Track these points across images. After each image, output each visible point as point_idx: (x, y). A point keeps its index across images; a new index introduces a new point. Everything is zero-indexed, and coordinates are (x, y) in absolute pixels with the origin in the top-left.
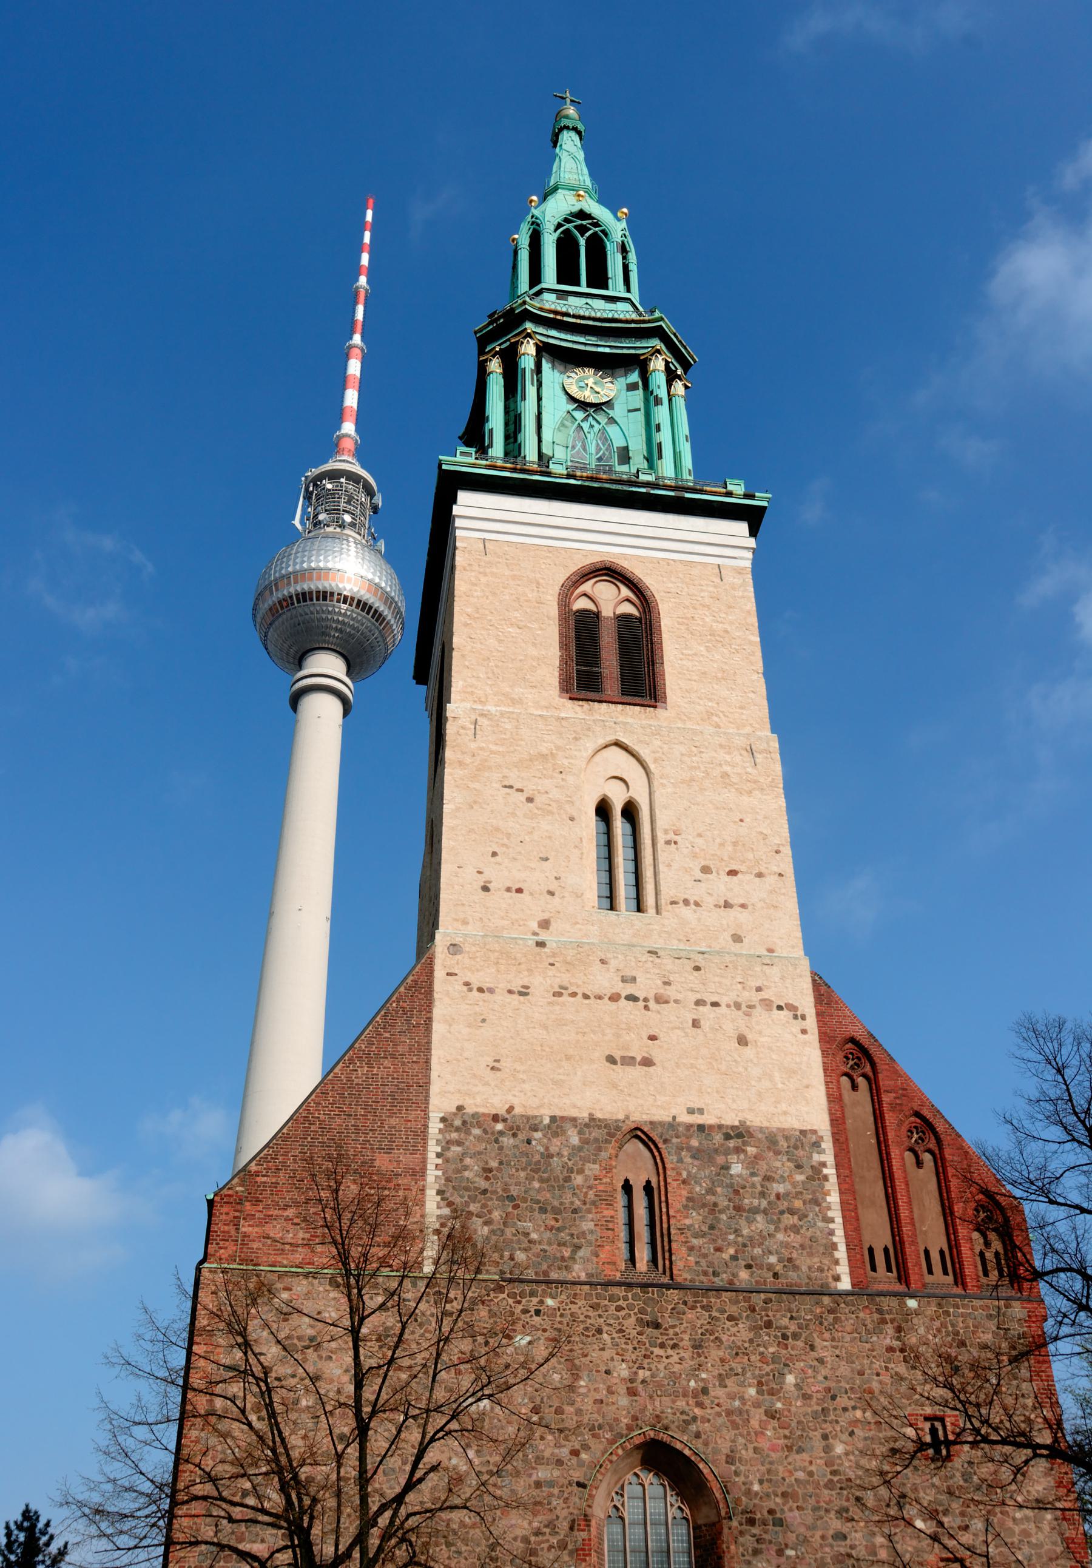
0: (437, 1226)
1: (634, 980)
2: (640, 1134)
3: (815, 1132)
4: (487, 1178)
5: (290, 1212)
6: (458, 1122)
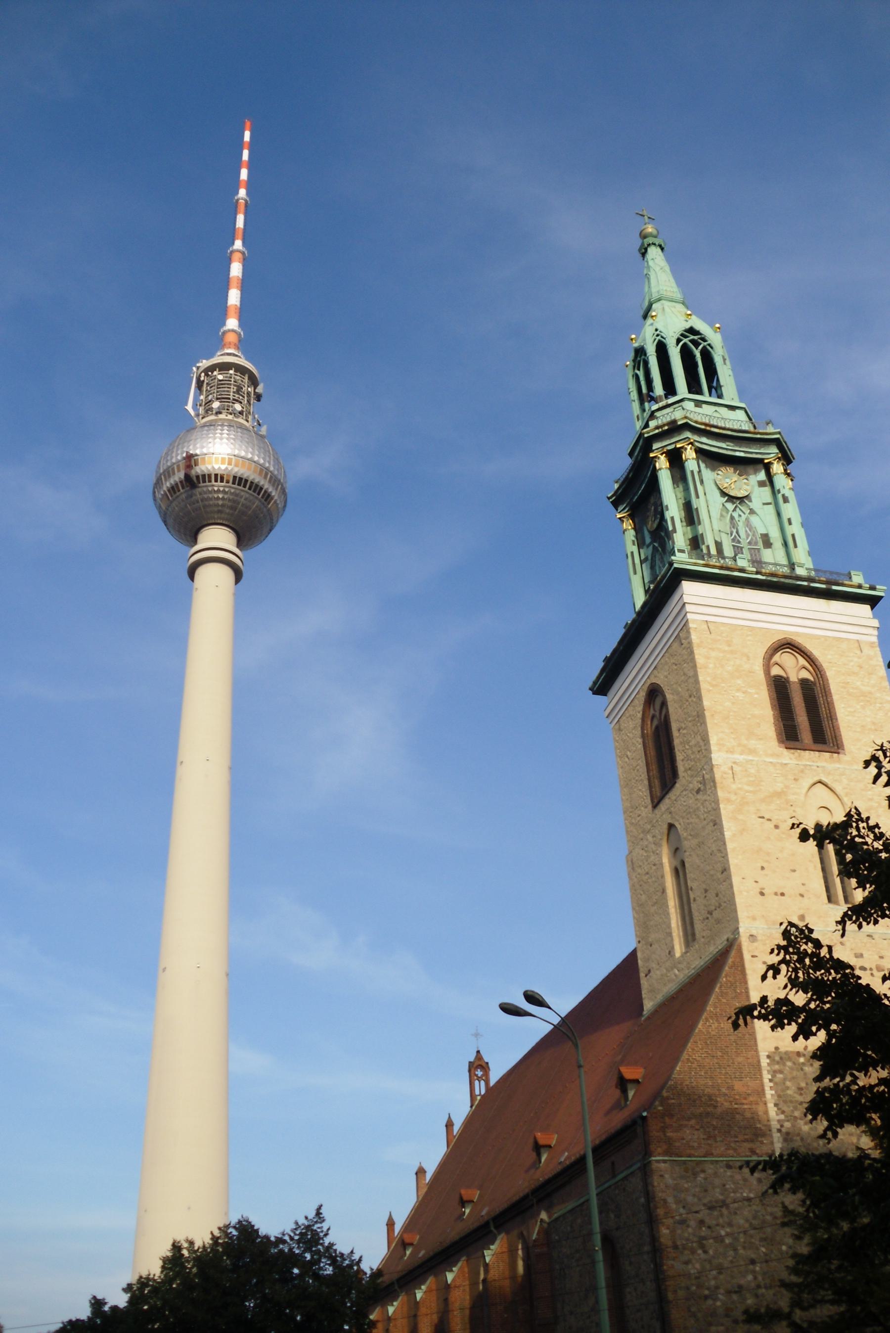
0: (779, 1127)
1: (861, 956)
4: (801, 1094)
5: (693, 1122)
6: (777, 1058)
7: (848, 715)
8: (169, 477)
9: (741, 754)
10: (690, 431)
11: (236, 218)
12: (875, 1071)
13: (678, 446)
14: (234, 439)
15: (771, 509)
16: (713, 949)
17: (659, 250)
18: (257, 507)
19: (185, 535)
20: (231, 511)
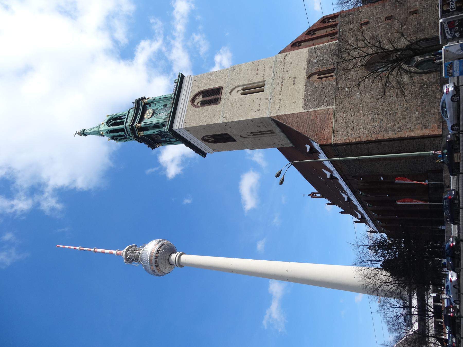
0: (325, 107)
2: (309, 77)
3: (309, 50)
4: (316, 100)
5: (322, 131)
6: (306, 107)
13: (137, 128)
16: (275, 125)
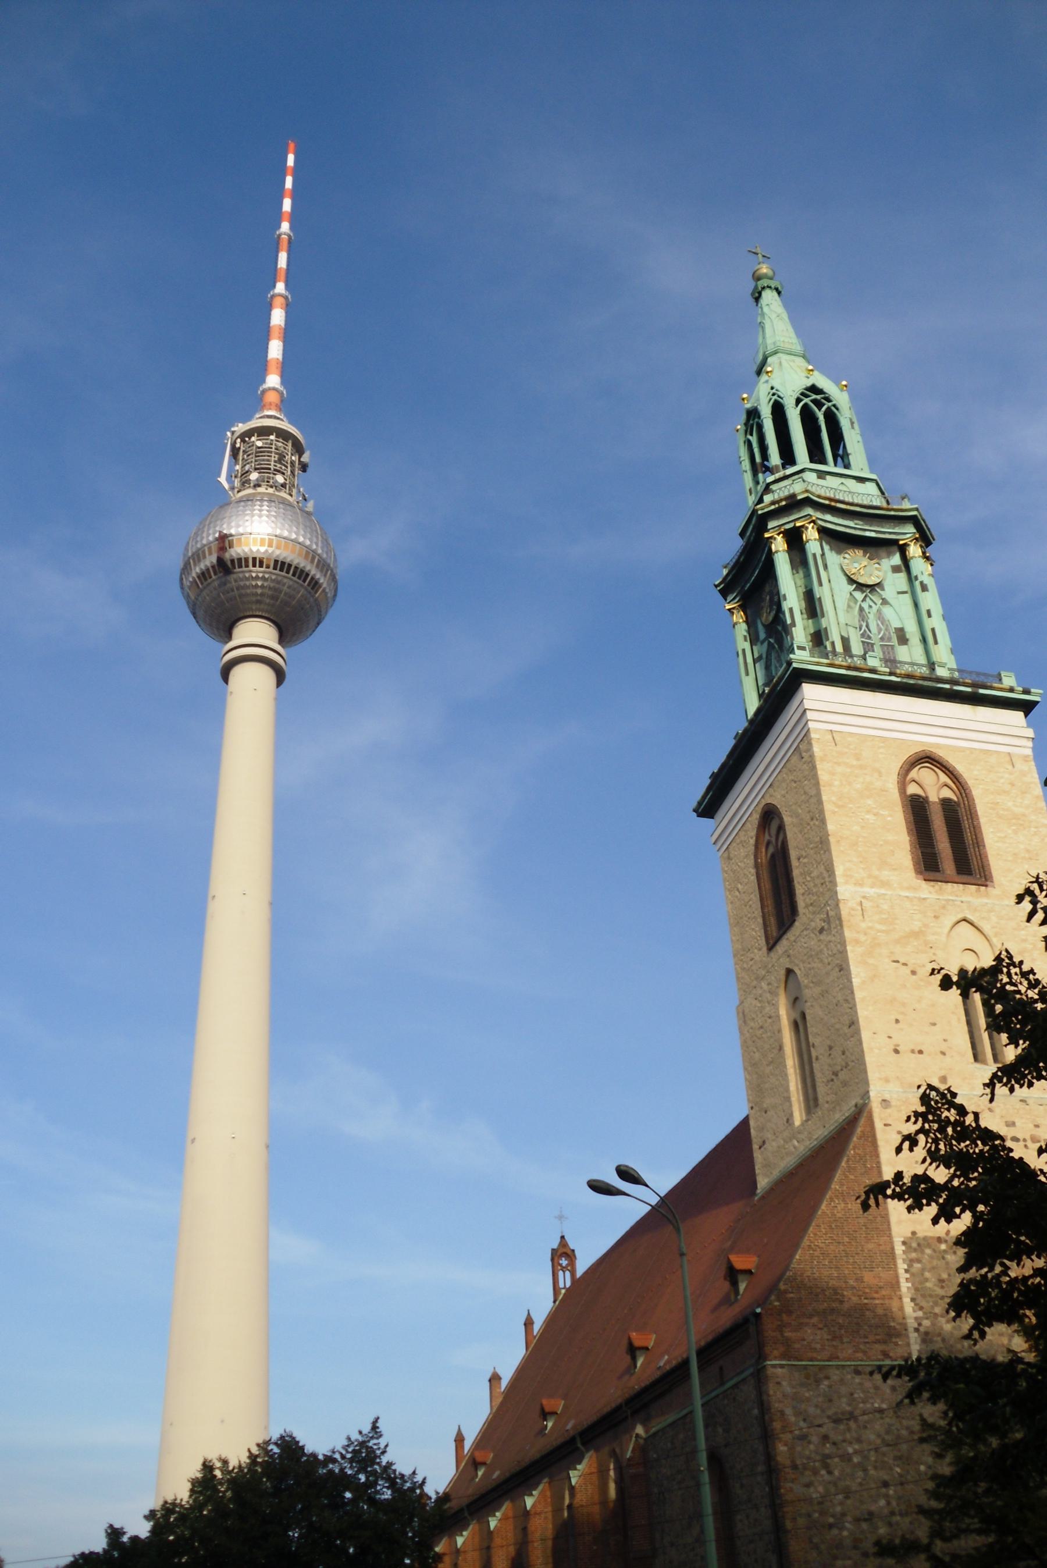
0: (916, 1325)
1: (1013, 1124)
4: (942, 1287)
5: (815, 1320)
6: (914, 1245)
7: (997, 842)
8: (199, 561)
9: (872, 887)
10: (812, 507)
11: (277, 256)
12: (1029, 1260)
13: (798, 524)
14: (275, 517)
15: (907, 599)
16: (839, 1117)
17: (775, 294)
18: (302, 596)
19: (218, 629)
20: (272, 602)
